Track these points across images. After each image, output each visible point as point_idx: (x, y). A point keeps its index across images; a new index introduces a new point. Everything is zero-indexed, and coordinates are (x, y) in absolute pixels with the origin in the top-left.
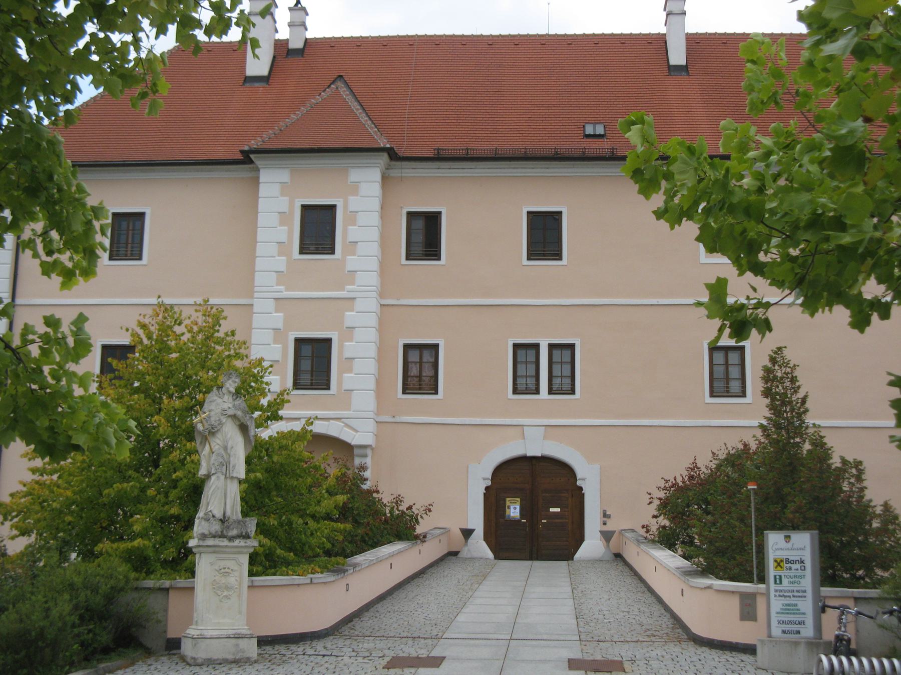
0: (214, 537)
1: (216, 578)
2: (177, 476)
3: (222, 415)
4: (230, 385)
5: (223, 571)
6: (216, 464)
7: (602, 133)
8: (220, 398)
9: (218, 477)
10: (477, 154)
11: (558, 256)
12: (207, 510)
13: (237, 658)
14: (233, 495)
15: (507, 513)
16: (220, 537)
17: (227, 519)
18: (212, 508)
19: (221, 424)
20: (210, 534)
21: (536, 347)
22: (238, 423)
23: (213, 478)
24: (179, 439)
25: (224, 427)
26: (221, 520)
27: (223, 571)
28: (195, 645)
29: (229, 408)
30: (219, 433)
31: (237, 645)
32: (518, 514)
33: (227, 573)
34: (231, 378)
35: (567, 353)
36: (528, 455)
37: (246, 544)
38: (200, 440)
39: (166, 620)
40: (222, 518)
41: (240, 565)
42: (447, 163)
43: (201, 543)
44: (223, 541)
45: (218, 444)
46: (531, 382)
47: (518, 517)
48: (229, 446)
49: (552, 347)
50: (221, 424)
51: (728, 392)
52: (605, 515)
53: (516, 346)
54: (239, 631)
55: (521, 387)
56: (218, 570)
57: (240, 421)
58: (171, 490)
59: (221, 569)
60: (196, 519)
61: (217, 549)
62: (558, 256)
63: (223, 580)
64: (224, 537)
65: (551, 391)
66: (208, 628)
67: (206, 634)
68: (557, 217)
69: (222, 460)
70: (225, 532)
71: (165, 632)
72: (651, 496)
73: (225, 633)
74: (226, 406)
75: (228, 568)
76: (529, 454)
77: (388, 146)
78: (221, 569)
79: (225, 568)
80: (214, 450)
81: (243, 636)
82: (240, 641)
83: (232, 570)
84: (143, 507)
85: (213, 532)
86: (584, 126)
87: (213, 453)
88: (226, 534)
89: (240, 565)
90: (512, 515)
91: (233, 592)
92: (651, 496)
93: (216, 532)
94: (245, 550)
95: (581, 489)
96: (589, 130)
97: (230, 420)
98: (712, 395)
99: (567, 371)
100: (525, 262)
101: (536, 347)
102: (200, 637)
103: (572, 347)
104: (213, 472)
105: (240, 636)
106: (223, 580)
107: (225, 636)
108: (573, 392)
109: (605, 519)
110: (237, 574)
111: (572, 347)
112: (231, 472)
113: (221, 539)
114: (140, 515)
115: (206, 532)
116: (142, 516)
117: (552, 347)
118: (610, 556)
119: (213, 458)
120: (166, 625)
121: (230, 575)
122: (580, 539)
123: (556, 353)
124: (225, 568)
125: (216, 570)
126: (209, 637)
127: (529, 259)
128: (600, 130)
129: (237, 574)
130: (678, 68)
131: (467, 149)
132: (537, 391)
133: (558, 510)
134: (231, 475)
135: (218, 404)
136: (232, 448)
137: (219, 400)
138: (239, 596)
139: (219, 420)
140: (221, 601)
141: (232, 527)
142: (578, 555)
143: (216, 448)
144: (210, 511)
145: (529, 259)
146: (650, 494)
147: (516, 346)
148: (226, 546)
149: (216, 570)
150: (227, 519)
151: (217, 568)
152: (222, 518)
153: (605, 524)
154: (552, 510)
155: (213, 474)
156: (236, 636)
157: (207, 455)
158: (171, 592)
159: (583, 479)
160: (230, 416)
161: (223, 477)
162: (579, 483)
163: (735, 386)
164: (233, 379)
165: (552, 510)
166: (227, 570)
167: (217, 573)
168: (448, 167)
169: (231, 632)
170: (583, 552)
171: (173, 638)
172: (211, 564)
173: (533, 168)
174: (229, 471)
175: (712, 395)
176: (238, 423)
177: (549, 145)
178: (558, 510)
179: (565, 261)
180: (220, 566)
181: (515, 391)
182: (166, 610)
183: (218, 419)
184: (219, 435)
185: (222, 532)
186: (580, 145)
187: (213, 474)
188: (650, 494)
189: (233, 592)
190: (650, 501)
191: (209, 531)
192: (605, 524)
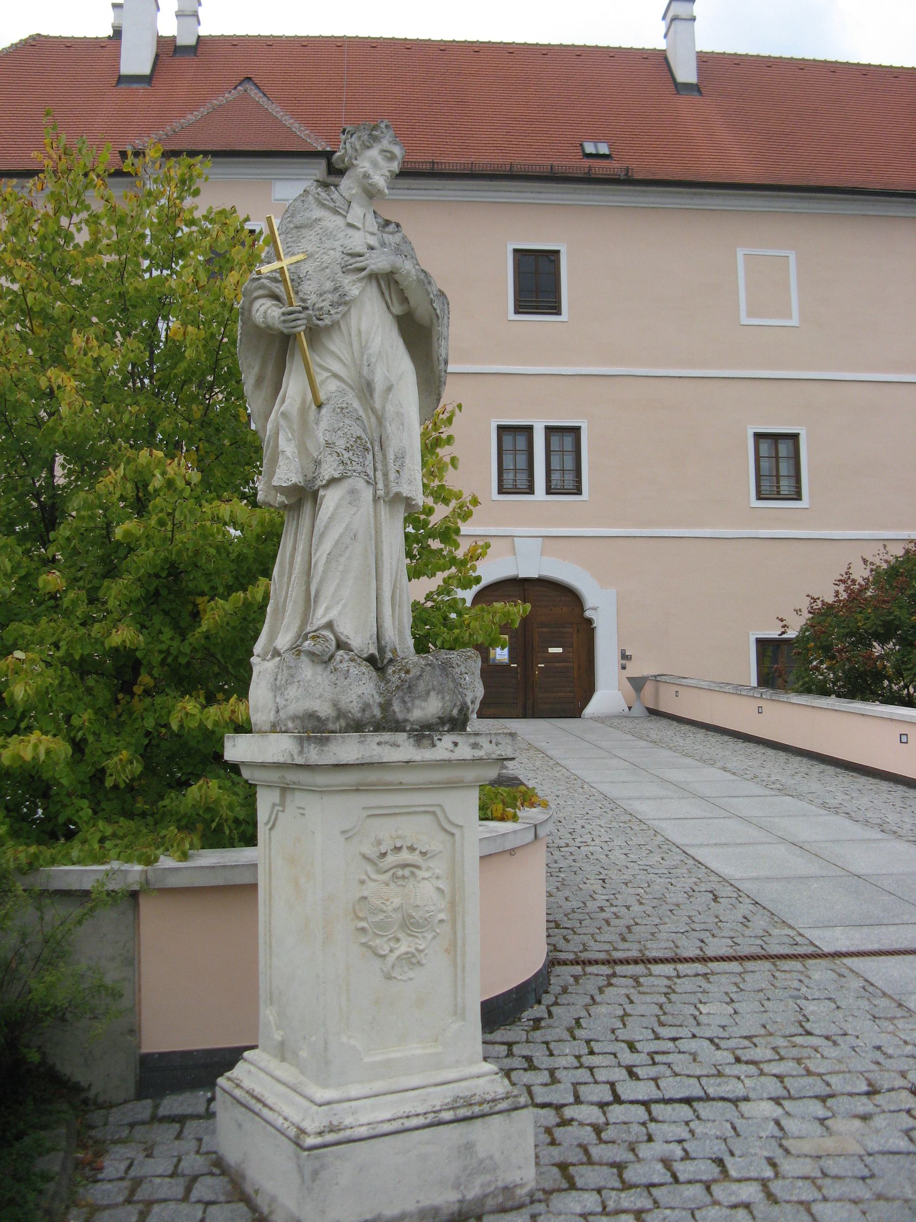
0: (357, 727)
1: (369, 890)
2: (127, 534)
3: (346, 270)
4: (375, 164)
5: (391, 859)
6: (341, 443)
7: (607, 152)
8: (336, 212)
9: (353, 492)
10: (447, 169)
11: (555, 309)
12: (305, 621)
13: (470, 1196)
14: (394, 564)
15: (492, 656)
16: (379, 727)
17: (389, 655)
18: (333, 614)
19: (343, 301)
20: (341, 714)
21: (529, 430)
22: (397, 309)
23: (331, 499)
24: (115, 447)
25: (354, 312)
26: (371, 660)
27: (391, 859)
28: (315, 1173)
29: (371, 248)
30: (336, 336)
31: (469, 1147)
32: (506, 657)
33: (405, 866)
34: (376, 139)
35: (568, 441)
36: (520, 576)
37: (479, 753)
38: (256, 370)
39: (137, 990)
40: (373, 650)
41: (449, 830)
42: (406, 181)
43: (314, 755)
44: (395, 745)
45: (336, 376)
46: (522, 477)
47: (507, 661)
48: (379, 385)
49: (549, 430)
50: (343, 301)
51: (778, 493)
52: (625, 656)
53: (502, 429)
54: (461, 1090)
55: (508, 484)
56: (374, 856)
57: (405, 300)
58: (106, 583)
59: (384, 855)
60: (254, 660)
61: (372, 776)
62: (555, 309)
63: (395, 897)
64: (397, 726)
65: (549, 492)
66: (354, 1093)
67: (347, 1121)
68: (553, 258)
69: (359, 432)
70: (396, 707)
71: (134, 1031)
72: (784, 623)
73: (413, 1104)
74: (358, 241)
75: (412, 849)
76: (523, 575)
77: (328, 149)
78: (384, 855)
79: (398, 849)
80: (322, 396)
81: (486, 1108)
82: (478, 1132)
83: (423, 854)
84: (27, 629)
85: (354, 708)
86: (581, 145)
87: (320, 406)
88: (400, 716)
89: (449, 830)
90: (498, 657)
91: (429, 936)
92: (784, 623)
93: (365, 707)
94: (470, 775)
95: (589, 621)
96: (590, 148)
97: (372, 291)
98: (759, 498)
99: (569, 464)
100: (512, 316)
101: (529, 430)
102: (330, 1137)
103: (576, 430)
104: (329, 470)
105: (477, 1109)
106: (395, 897)
107: (421, 1121)
108: (578, 491)
109: (624, 662)
110: (439, 866)
111: (576, 430)
112: (392, 476)
113: (387, 736)
114: (25, 649)
115: (324, 710)
116: (31, 655)
117: (549, 430)
118: (638, 710)
119: (324, 425)
120: (134, 1010)
121: (420, 874)
122: (588, 690)
123: (555, 440)
124: (398, 849)
125: (365, 857)
126: (363, 1131)
127: (517, 312)
128: (604, 149)
129: (439, 866)
130: (687, 87)
131: (433, 163)
132: (530, 490)
133: (560, 650)
134: (394, 489)
135: (328, 234)
136: (389, 389)
137: (333, 222)
138: (453, 949)
139: (336, 289)
140: (389, 977)
141: (422, 686)
142: (590, 710)
143: (329, 388)
144: (330, 626)
145: (517, 312)
146: (782, 620)
147: (502, 429)
148: (408, 764)
149: (365, 857)
150: (389, 655)
151: (369, 850)
152: (373, 650)
153: (624, 668)
154: (551, 650)
155: (333, 481)
156: (462, 1112)
157: (294, 413)
158: (145, 904)
159: (595, 609)
160: (374, 277)
161: (367, 494)
162: (588, 614)
163: (786, 486)
164: (385, 144)
165: (551, 650)
166: (405, 856)
167: (369, 868)
168: (406, 186)
169: (438, 1098)
170: (597, 705)
171: (162, 1055)
172: (348, 835)
173: (520, 192)
174: (386, 475)
175: (759, 498)
176: (397, 309)
177: (541, 162)
178: (560, 650)
179: (564, 317)
180: (379, 843)
181: (501, 491)
182: (132, 961)
183: (329, 285)
184: (335, 344)
185: (385, 707)
186: (577, 165)
187: (333, 481)
188: (782, 620)
189: (429, 936)
190: (783, 630)
191: (335, 705)
192: (624, 668)
